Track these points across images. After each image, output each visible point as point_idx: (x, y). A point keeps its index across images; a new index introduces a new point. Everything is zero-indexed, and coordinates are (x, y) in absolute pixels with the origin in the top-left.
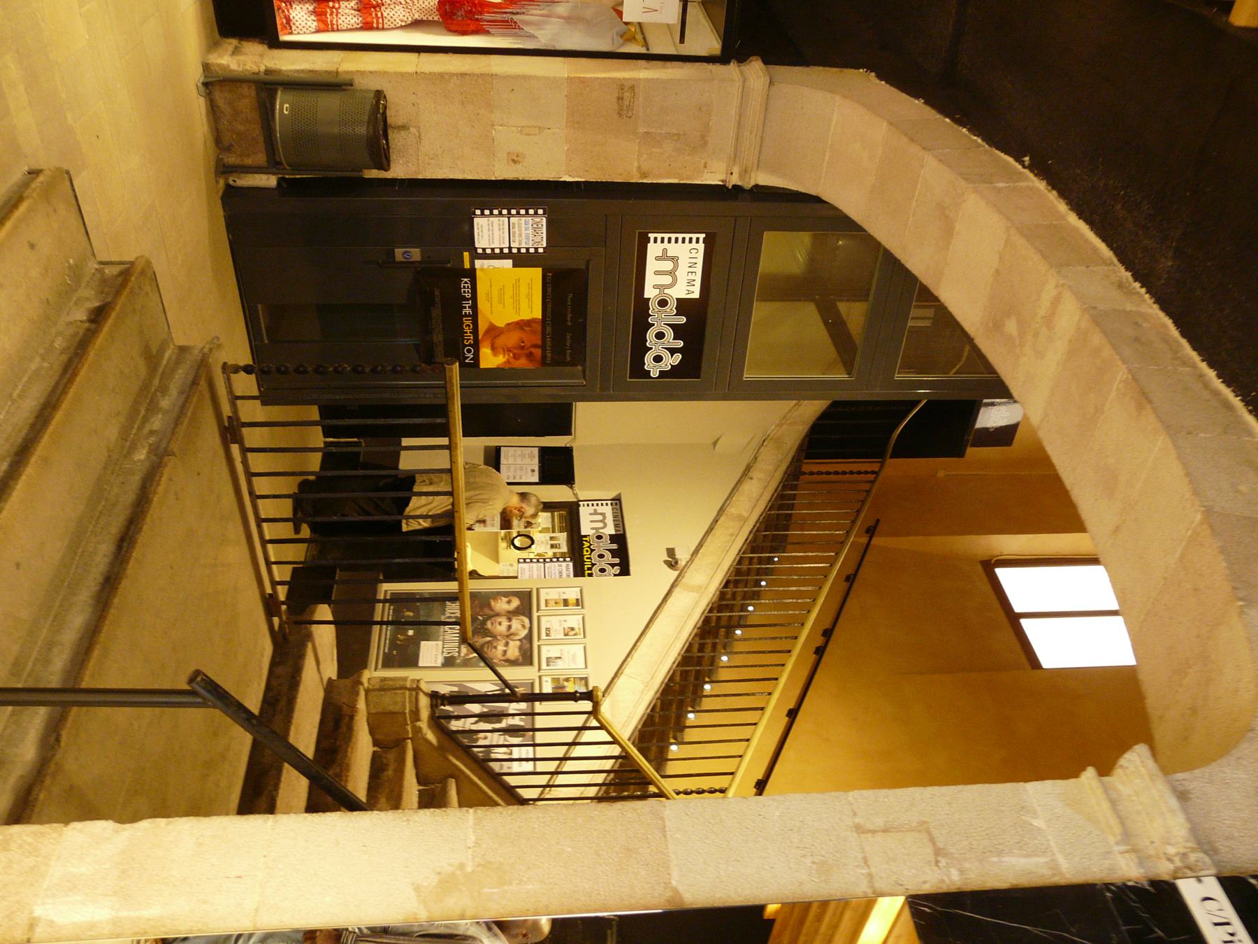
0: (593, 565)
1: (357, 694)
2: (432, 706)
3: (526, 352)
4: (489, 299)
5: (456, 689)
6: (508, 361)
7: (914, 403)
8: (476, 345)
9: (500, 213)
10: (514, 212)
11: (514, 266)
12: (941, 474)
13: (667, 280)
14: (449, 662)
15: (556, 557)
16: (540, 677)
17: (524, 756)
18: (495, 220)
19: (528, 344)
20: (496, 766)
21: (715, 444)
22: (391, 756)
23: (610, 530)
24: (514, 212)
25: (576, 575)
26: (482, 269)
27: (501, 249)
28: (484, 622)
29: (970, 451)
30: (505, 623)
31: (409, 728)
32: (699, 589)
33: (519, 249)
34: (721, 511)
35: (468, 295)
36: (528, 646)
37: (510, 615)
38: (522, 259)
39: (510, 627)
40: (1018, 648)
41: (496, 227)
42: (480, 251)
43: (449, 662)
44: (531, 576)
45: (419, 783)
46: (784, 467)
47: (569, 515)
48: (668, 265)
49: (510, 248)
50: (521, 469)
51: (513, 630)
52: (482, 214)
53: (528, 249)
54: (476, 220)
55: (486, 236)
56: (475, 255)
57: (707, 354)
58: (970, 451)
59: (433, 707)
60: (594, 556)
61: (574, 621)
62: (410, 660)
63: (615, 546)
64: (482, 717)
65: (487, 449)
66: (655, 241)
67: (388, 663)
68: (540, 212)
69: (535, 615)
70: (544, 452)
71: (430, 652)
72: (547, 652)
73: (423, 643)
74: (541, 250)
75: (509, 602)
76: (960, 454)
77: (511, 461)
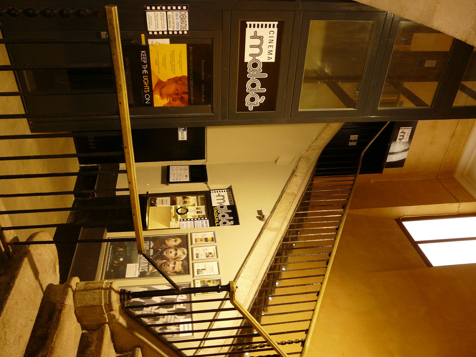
0: (219, 221)
1: (66, 294)
2: (121, 300)
3: (180, 96)
4: (157, 64)
5: (146, 290)
6: (170, 103)
7: (385, 123)
8: (151, 93)
9: (161, 9)
10: (169, 8)
11: (171, 42)
12: (372, 181)
13: (257, 51)
14: (143, 275)
15: (200, 218)
16: (194, 281)
17: (186, 330)
18: (159, 13)
19: (180, 91)
20: (169, 338)
21: (276, 161)
22: (95, 336)
23: (227, 203)
24: (169, 8)
25: (210, 226)
26: (152, 45)
27: (163, 32)
28: (162, 252)
29: (385, 170)
30: (174, 252)
31: (106, 316)
32: (277, 230)
33: (173, 32)
34: (283, 192)
35: (145, 62)
36: (187, 263)
37: (176, 248)
38: (175, 38)
39: (176, 254)
40: (418, 257)
41: (159, 18)
42: (151, 33)
43: (143, 275)
44: (187, 228)
45: (117, 351)
46: (311, 170)
47: (206, 198)
48: (257, 42)
49: (168, 31)
50: (180, 175)
51: (178, 255)
52: (151, 9)
53: (178, 32)
54: (148, 13)
55: (154, 24)
56: (149, 36)
57: (275, 109)
58: (385, 170)
59: (122, 300)
60: (220, 216)
61: (211, 249)
62: (121, 275)
63: (230, 211)
64: (161, 305)
65: (163, 168)
66: (250, 27)
67: (109, 276)
68: (185, 8)
69: (190, 247)
70: (192, 168)
71: (132, 270)
72: (197, 266)
73: (128, 265)
74: (186, 33)
75: (175, 241)
76: (380, 171)
77: (175, 172)
